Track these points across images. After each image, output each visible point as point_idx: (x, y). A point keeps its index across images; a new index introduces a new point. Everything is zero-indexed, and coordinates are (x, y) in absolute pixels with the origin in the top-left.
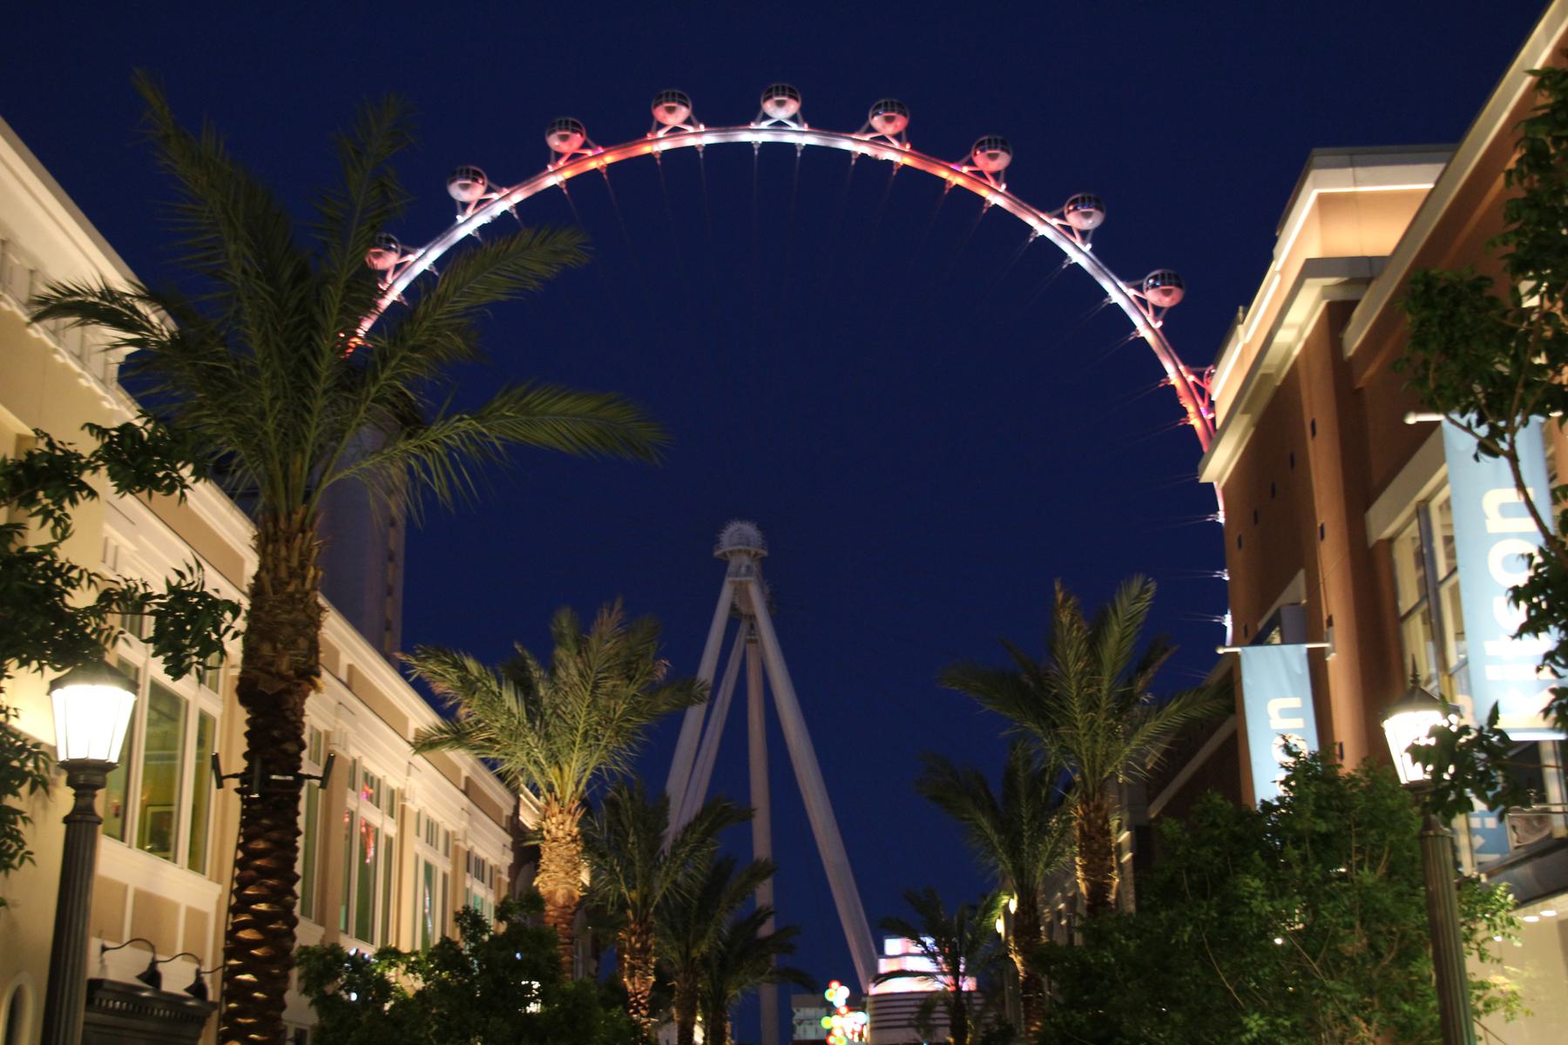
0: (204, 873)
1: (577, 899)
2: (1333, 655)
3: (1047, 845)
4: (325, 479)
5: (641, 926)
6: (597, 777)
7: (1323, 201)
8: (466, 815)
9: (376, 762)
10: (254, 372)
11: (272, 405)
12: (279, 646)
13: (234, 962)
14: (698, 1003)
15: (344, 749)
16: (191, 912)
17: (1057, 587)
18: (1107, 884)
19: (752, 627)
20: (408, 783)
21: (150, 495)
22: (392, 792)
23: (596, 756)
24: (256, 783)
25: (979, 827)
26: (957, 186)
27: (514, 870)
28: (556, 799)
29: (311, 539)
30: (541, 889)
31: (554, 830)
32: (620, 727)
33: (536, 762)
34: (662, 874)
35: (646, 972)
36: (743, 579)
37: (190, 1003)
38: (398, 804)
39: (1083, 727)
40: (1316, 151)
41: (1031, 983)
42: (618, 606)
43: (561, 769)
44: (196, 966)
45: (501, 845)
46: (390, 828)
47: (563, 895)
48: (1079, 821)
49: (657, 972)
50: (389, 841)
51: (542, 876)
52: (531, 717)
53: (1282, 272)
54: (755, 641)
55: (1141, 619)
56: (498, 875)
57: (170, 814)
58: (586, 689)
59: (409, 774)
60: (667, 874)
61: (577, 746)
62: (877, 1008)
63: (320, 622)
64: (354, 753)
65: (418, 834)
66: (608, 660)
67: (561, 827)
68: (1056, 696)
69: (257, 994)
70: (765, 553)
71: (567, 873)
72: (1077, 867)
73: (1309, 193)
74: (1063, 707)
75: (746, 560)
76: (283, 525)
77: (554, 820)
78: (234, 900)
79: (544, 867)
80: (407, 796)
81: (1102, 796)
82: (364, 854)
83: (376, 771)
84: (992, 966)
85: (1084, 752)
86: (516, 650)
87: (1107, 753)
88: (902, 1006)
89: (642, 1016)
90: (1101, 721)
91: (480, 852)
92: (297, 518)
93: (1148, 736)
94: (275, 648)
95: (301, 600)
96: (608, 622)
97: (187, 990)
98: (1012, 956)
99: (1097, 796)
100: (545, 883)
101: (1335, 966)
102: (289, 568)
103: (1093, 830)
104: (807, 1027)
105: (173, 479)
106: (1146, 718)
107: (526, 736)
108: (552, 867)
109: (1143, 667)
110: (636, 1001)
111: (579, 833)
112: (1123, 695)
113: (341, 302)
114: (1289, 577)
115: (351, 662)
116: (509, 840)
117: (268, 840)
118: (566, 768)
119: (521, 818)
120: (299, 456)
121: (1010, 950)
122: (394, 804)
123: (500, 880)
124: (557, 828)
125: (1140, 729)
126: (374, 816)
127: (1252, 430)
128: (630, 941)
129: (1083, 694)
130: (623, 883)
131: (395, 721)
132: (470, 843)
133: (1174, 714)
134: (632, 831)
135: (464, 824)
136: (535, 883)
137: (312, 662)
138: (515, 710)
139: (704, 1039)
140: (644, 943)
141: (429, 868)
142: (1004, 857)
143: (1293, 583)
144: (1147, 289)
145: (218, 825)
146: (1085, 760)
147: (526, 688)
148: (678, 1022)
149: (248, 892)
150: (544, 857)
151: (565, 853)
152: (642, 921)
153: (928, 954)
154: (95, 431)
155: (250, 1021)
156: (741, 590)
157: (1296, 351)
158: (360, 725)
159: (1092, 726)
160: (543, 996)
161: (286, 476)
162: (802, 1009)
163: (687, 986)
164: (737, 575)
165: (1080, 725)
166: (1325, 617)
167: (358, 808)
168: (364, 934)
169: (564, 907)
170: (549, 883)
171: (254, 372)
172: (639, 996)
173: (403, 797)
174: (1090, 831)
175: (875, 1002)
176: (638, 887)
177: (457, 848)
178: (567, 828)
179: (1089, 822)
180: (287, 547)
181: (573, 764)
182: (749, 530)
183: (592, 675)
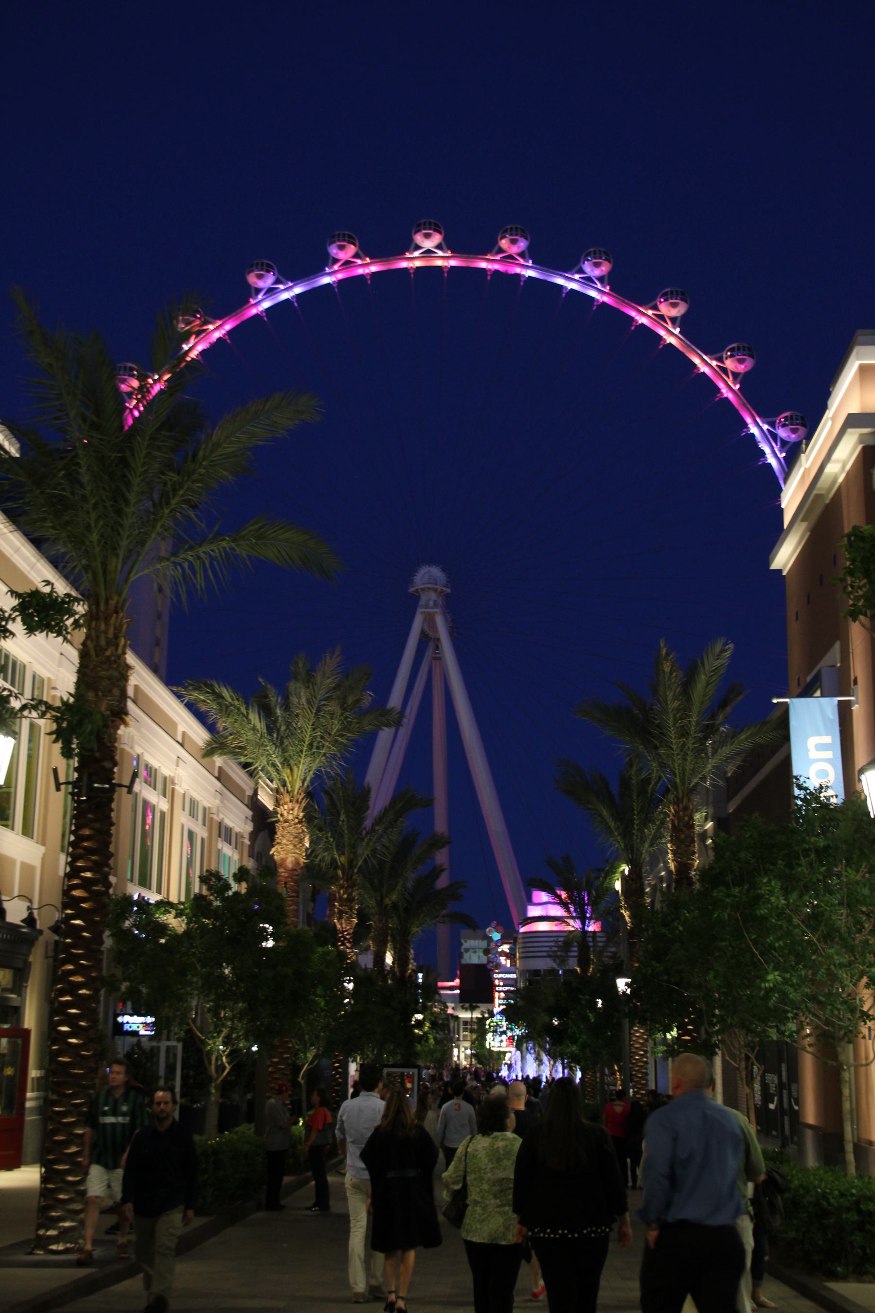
0: (32, 838)
1: (302, 864)
2: (857, 705)
3: (650, 831)
4: (132, 575)
5: (347, 882)
6: (318, 776)
7: (863, 369)
8: (219, 795)
9: (153, 757)
10: (84, 499)
11: (97, 521)
12: (100, 694)
13: (69, 911)
14: (389, 938)
15: (132, 748)
16: (24, 865)
17: (662, 644)
18: (690, 864)
19: (437, 647)
20: (177, 772)
21: (47, 635)
22: (165, 778)
23: (318, 761)
24: (84, 791)
25: (601, 815)
26: (642, 324)
27: (253, 836)
28: (288, 792)
29: (122, 618)
30: (276, 857)
31: (285, 814)
32: (336, 741)
33: (274, 765)
34: (364, 844)
35: (350, 915)
36: (431, 610)
37: (24, 930)
38: (169, 787)
39: (677, 749)
40: (859, 331)
41: (631, 933)
42: (338, 651)
43: (291, 770)
44: (29, 904)
45: (244, 817)
46: (163, 805)
47: (292, 862)
48: (672, 817)
49: (359, 916)
50: (163, 814)
51: (277, 847)
52: (270, 730)
53: (833, 419)
54: (439, 659)
55: (722, 671)
56: (241, 840)
57: (9, 794)
58: (312, 712)
59: (177, 765)
60: (368, 844)
61: (304, 753)
62: (524, 943)
63: (128, 676)
64: (138, 750)
65: (184, 810)
66: (328, 692)
67: (291, 812)
68: (658, 726)
69: (84, 934)
70: (449, 590)
71: (295, 846)
72: (669, 851)
73: (854, 363)
74: (662, 734)
75: (433, 596)
76: (102, 607)
77: (286, 807)
78: (68, 869)
79: (278, 841)
80: (176, 782)
81: (689, 800)
82: (144, 823)
83: (154, 763)
84: (610, 919)
85: (677, 768)
86: (260, 683)
87: (694, 769)
88: (530, 952)
89: (347, 947)
90: (690, 745)
91: (229, 823)
92: (112, 603)
93: (724, 756)
94: (97, 695)
95: (115, 661)
96: (330, 664)
97: (23, 921)
98: (623, 911)
99: (685, 800)
100: (279, 852)
101: (828, 937)
102: (107, 638)
103: (681, 824)
104: (473, 954)
105: (61, 627)
106: (722, 743)
107: (266, 746)
108: (284, 841)
109: (723, 705)
110: (343, 937)
111: (304, 816)
112: (707, 726)
113: (145, 457)
114: (830, 645)
115: (137, 683)
116: (250, 813)
117: (91, 829)
118: (295, 769)
119: (259, 797)
120: (114, 559)
121: (621, 907)
122: (167, 788)
123: (243, 843)
124: (288, 813)
125: (719, 750)
126: (152, 796)
127: (808, 534)
128: (339, 893)
129: (677, 725)
130: (335, 850)
131: (167, 726)
132: (221, 816)
133: (745, 741)
134: (343, 811)
135: (217, 802)
136: (271, 852)
137: (122, 705)
138: (258, 726)
139: (393, 963)
140: (350, 895)
141: (191, 834)
142: (619, 838)
143: (832, 650)
144: (727, 359)
145: (43, 804)
146: (677, 773)
147: (266, 711)
148: (374, 951)
149: (79, 864)
150: (278, 833)
151: (294, 831)
152: (348, 878)
153: (564, 905)
154: (14, 595)
155: (80, 952)
156: (430, 620)
157: (840, 480)
158: (143, 729)
159: (684, 748)
160: (275, 936)
161: (105, 572)
162: (468, 941)
163: (381, 925)
164: (427, 607)
165: (674, 747)
166: (852, 678)
167: (140, 791)
168: (144, 882)
169: (293, 870)
170: (282, 853)
171: (84, 499)
172: (346, 933)
173: (173, 783)
174: (678, 825)
175: (524, 938)
176: (346, 853)
177: (212, 819)
178: (295, 813)
179: (679, 819)
180: (106, 624)
181: (301, 766)
182: (436, 572)
183: (317, 702)
